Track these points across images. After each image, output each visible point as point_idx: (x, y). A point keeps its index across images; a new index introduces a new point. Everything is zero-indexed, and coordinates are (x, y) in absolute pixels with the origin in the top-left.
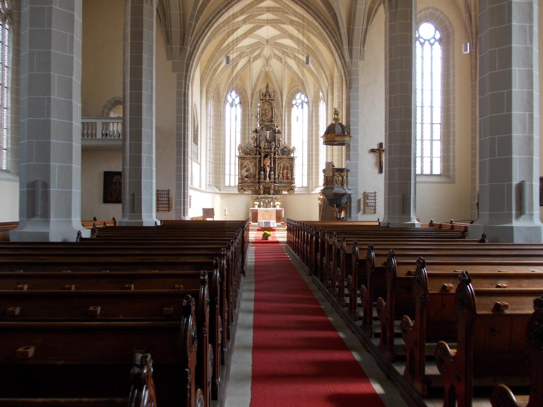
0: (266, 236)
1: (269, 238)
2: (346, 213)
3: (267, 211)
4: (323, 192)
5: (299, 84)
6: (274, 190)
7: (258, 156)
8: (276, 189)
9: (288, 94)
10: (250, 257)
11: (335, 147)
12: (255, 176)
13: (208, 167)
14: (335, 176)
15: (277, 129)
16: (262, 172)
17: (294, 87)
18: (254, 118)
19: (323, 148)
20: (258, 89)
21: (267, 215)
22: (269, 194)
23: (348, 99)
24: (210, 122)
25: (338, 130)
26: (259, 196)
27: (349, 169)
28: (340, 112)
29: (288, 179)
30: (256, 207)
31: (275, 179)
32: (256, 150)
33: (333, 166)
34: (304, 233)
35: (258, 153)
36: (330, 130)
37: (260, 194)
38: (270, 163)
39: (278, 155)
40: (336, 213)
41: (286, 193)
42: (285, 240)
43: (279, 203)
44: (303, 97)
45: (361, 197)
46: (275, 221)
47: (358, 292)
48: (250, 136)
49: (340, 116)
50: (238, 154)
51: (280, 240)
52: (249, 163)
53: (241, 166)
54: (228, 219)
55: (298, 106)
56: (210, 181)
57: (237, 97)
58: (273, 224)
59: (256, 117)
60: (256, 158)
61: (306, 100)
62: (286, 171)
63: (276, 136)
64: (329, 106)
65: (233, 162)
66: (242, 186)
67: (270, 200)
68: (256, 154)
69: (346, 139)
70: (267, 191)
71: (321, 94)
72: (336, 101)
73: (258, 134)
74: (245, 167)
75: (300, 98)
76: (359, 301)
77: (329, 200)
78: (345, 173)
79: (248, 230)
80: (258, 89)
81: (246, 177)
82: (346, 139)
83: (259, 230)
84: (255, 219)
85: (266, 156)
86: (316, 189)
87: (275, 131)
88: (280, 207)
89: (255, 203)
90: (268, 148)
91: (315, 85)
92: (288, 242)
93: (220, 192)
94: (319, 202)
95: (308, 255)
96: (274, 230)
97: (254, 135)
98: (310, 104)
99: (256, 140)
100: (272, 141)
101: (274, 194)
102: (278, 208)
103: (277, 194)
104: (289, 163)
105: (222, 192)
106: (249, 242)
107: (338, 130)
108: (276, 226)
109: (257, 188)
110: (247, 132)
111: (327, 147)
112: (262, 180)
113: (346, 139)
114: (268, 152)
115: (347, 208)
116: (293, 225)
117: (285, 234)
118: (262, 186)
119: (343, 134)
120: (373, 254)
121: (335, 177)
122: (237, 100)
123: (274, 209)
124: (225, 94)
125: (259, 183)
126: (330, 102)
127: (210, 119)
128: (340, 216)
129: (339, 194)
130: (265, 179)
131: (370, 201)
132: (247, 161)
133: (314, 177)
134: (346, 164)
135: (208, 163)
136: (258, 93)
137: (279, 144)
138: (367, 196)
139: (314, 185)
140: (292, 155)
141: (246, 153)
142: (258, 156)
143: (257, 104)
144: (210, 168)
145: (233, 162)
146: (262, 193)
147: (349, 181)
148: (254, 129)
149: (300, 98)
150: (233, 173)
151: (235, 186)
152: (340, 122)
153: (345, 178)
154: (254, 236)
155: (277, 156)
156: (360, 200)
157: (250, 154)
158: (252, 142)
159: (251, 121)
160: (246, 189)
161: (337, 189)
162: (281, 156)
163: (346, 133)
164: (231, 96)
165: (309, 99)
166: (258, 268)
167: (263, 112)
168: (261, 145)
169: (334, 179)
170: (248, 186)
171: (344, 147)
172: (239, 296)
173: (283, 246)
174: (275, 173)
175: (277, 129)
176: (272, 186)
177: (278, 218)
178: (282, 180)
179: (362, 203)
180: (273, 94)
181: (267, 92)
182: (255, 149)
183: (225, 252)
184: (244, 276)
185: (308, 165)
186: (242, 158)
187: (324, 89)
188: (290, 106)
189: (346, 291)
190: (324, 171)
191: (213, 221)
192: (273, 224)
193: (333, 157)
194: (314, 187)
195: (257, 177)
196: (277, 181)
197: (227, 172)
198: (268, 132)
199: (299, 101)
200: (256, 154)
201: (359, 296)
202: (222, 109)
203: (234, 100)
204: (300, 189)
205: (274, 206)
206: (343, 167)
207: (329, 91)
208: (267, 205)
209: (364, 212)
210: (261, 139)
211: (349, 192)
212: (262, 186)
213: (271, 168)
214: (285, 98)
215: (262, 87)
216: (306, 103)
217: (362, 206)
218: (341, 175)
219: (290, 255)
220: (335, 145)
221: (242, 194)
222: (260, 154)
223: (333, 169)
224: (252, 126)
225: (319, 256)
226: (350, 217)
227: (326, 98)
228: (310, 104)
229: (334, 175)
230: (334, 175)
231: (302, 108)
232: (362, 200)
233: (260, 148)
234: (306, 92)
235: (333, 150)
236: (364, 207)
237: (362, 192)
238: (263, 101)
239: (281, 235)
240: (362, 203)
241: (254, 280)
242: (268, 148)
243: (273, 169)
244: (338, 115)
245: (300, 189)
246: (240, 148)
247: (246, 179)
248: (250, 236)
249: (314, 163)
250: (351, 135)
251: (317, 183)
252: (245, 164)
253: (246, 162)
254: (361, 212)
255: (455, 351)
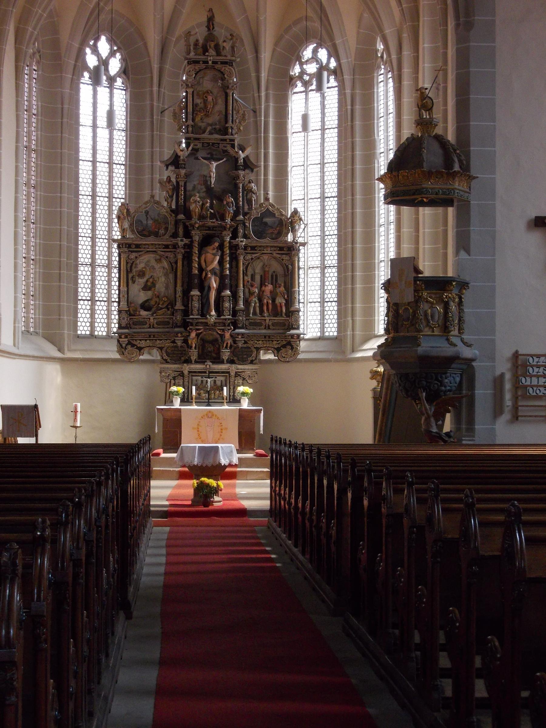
0: (204, 494)
1: (216, 498)
2: (457, 420)
3: (210, 415)
4: (384, 354)
5: (311, 13)
6: (234, 349)
7: (181, 242)
8: (240, 345)
9: (276, 44)
10: (152, 559)
11: (425, 212)
12: (172, 304)
13: (22, 277)
14: (422, 301)
15: (242, 155)
16: (195, 293)
17: (296, 23)
18: (168, 118)
19: (385, 213)
20: (180, 30)
21: (211, 428)
22: (218, 360)
23: (463, 59)
24: (29, 133)
25: (432, 157)
26: (186, 368)
27: (467, 279)
28: (438, 101)
29: (276, 312)
30: (177, 404)
31: (235, 313)
32: (177, 222)
33: (417, 271)
34: (281, 460)
35: (181, 231)
36: (407, 156)
37: (188, 361)
38: (221, 263)
39: (245, 236)
40: (428, 419)
41: (270, 356)
42: (265, 504)
43: (249, 390)
44: (323, 54)
45: (503, 367)
46: (233, 446)
47: (478, 662)
48: (157, 176)
49: (437, 115)
50: (117, 235)
51: (248, 504)
52: (153, 263)
53: (128, 273)
54: (86, 437)
55: (306, 84)
56: (27, 318)
57: (112, 54)
58: (229, 453)
59: (176, 116)
60: (175, 246)
61: (333, 64)
62: (270, 287)
63: (238, 177)
64: (406, 83)
65: (102, 257)
66: (132, 335)
67: (220, 379)
68: (175, 235)
69: (458, 185)
70: (210, 352)
71: (380, 47)
72: (426, 66)
73: (183, 172)
74: (142, 274)
75: (315, 58)
76: (480, 689)
77: (404, 377)
78: (455, 291)
79: (148, 476)
80: (180, 30)
81: (145, 306)
82: (456, 185)
83: (182, 476)
84: (172, 441)
85: (206, 242)
86: (366, 346)
87: (236, 159)
88: (252, 402)
89: (174, 388)
90: (213, 216)
91: (360, 19)
92: (274, 512)
93: (59, 355)
94: (374, 383)
95: (333, 549)
96: (232, 476)
97: (169, 173)
98: (347, 77)
99: (176, 188)
100: (225, 192)
101: (231, 362)
102: (245, 404)
103: (243, 361)
104: (280, 261)
105: (69, 355)
106: (147, 512)
107: (432, 157)
108: (235, 461)
109: (179, 343)
110: (147, 163)
111: (398, 213)
112: (195, 316)
113: (456, 185)
114: (209, 228)
115: (461, 402)
116: (288, 457)
117: (264, 487)
118: (193, 335)
119: (447, 171)
120: (520, 537)
121: (424, 306)
122: (115, 65)
123: (234, 408)
124: (76, 45)
125: (185, 325)
126: (407, 70)
127: (29, 124)
128: (441, 427)
129: (437, 358)
130: (204, 311)
131: (535, 381)
132: (146, 257)
133: (358, 305)
134: (458, 265)
135: (22, 262)
136: (182, 42)
137: (249, 202)
138: (525, 365)
139: (358, 333)
140: (290, 238)
141: (144, 232)
142: (181, 242)
143: (178, 76)
144: (27, 277)
145: (102, 257)
146: (194, 358)
147: (466, 318)
148: (167, 154)
149: (314, 56)
150: (101, 293)
151: (108, 337)
152: (439, 131)
153: (453, 307)
154: (167, 492)
155: (242, 242)
156: (502, 375)
157: (156, 235)
158: (160, 195)
159: (161, 129)
160: (143, 344)
161: (430, 344)
162: (254, 241)
163: (457, 168)
164: (95, 51)
165: (344, 61)
166: (176, 593)
167: (198, 101)
168: (192, 207)
169: (421, 312)
170: (151, 337)
171: (450, 210)
172: (106, 680)
173: (260, 524)
174: (235, 296)
175: (242, 155)
176: (227, 335)
177: (246, 439)
178: (258, 317)
179: (508, 386)
180: (228, 46)
181: (210, 37)
182: (171, 219)
183: (48, 532)
184: (129, 616)
185: (341, 268)
186: (129, 246)
187: (389, 31)
188: (284, 84)
189: (444, 661)
190: (388, 286)
191: (37, 446)
192: (229, 453)
193: (417, 242)
194: (358, 340)
195: (179, 306)
196: (241, 318)
197: (84, 292)
198: (215, 164)
199: (312, 68)
200: (175, 235)
201: (479, 676)
202: (67, 91)
203: (104, 63)
204: (315, 346)
205: (234, 400)
206: (450, 274)
207: (405, 35)
208: (209, 397)
209: (515, 417)
210: (190, 187)
211: (467, 353)
212: (193, 335)
213: (222, 278)
214: (266, 56)
215: (193, 21)
216: (334, 72)
217: (508, 396)
218: (441, 300)
219: (278, 553)
220: (422, 204)
221: (130, 361)
222: (187, 234)
223: (416, 279)
224: (161, 146)
225: (363, 554)
226: (471, 429)
227: (394, 57)
228: (347, 77)
229: (418, 300)
230: (418, 300)
231: (319, 88)
232: (508, 376)
233: (188, 214)
234: (332, 39)
235: (417, 220)
236: (515, 398)
237: (508, 353)
238: (197, 67)
239: (252, 492)
240: (508, 386)
241: (158, 630)
242: (213, 216)
243: (229, 282)
244: (430, 110)
245: (315, 346)
246: (125, 214)
247: (144, 313)
248: (153, 492)
249: (359, 262)
250: (473, 173)
251: (369, 324)
252: (141, 266)
253: (143, 261)
254: (506, 416)
255: (485, 695)
